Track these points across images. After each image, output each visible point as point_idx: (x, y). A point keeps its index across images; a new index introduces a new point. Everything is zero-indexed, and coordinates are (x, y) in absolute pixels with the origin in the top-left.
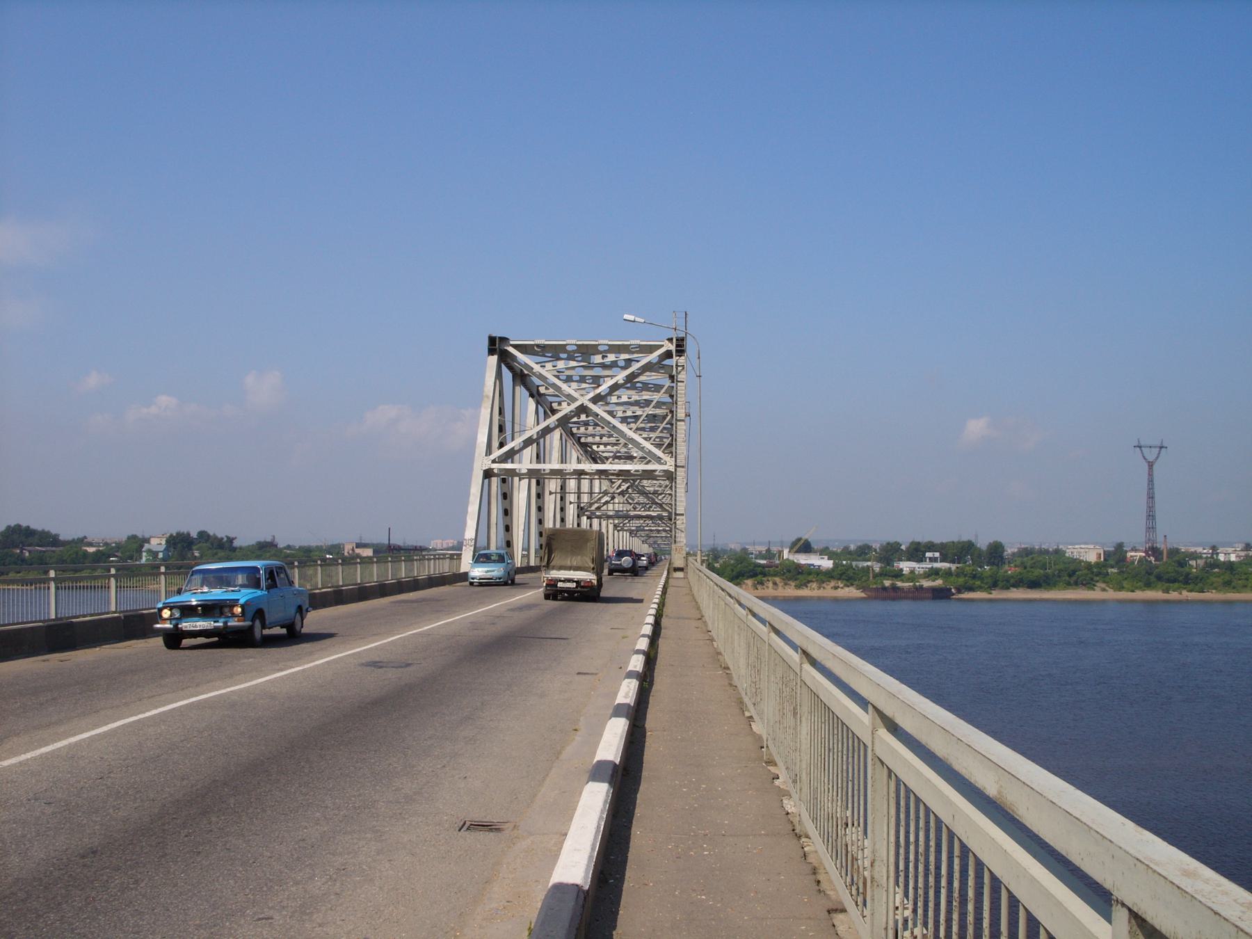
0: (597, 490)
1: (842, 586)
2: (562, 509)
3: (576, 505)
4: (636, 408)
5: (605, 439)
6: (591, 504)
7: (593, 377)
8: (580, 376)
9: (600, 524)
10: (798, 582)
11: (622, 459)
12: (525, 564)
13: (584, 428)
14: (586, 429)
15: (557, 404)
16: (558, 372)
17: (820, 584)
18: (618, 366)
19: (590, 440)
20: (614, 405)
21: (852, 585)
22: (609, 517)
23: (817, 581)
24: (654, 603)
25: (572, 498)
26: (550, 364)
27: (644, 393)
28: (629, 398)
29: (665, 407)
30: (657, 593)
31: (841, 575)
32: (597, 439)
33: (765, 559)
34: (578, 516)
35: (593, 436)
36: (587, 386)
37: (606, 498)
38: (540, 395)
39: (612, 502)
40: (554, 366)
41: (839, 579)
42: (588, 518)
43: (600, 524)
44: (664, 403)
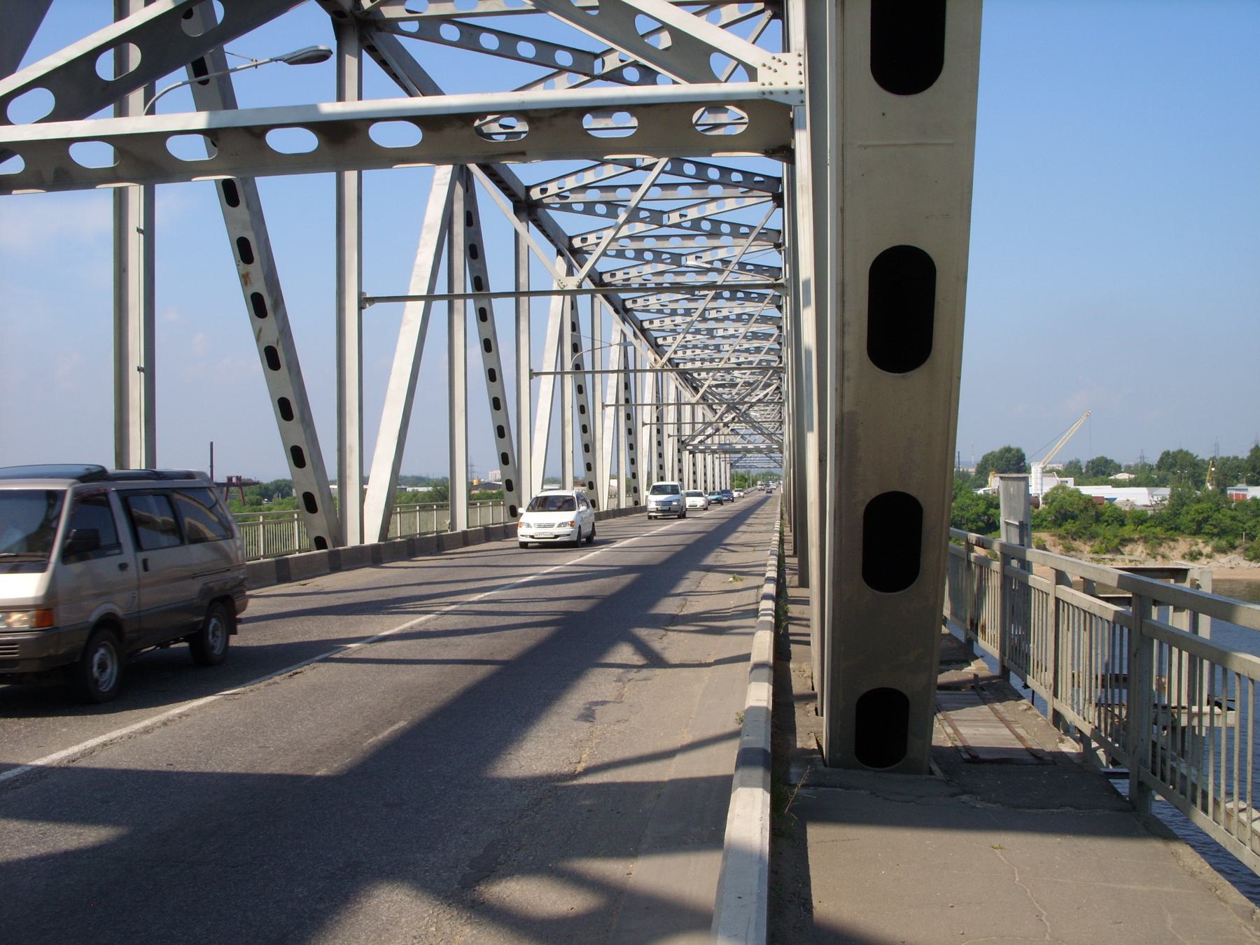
0: (699, 418)
1: (1207, 550)
2: (659, 443)
3: (676, 438)
4: (746, 355)
5: (707, 365)
6: (693, 437)
7: (707, 329)
8: (684, 309)
9: (705, 459)
10: (1097, 543)
11: (727, 387)
12: (613, 506)
13: (681, 352)
14: (685, 353)
15: (662, 339)
16: (662, 305)
17: (1153, 547)
18: (723, 298)
19: (689, 365)
20: (720, 338)
21: (1233, 547)
22: (714, 452)
23: (1145, 540)
24: (774, 541)
25: (670, 429)
26: (681, 352)
27: (754, 341)
28: (735, 331)
29: (771, 323)
30: (774, 538)
31: (1199, 524)
32: (698, 364)
33: (1133, 474)
34: (679, 451)
35: (693, 360)
36: (702, 337)
37: (709, 431)
38: (658, 346)
39: (717, 433)
40: (658, 300)
41: (1197, 532)
42: (690, 453)
43: (705, 459)
44: (771, 318)
